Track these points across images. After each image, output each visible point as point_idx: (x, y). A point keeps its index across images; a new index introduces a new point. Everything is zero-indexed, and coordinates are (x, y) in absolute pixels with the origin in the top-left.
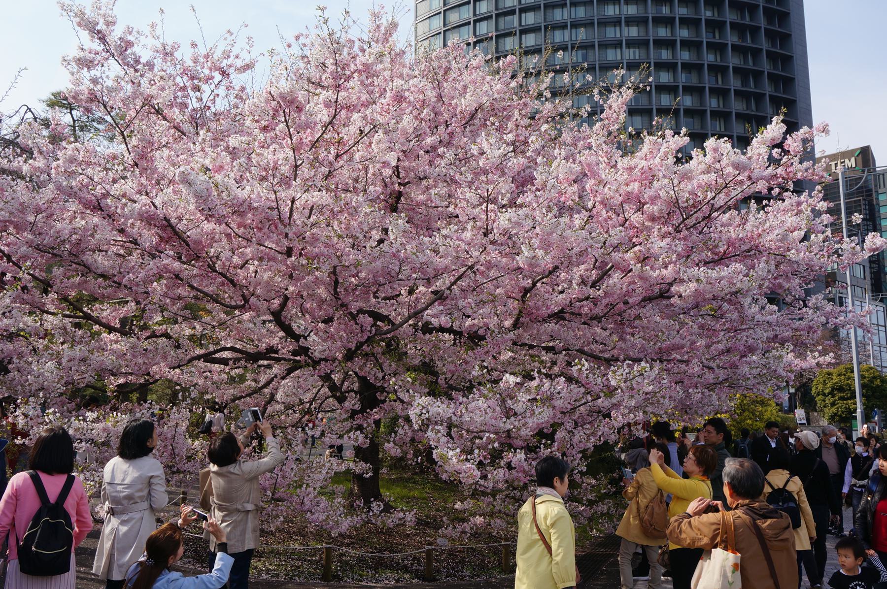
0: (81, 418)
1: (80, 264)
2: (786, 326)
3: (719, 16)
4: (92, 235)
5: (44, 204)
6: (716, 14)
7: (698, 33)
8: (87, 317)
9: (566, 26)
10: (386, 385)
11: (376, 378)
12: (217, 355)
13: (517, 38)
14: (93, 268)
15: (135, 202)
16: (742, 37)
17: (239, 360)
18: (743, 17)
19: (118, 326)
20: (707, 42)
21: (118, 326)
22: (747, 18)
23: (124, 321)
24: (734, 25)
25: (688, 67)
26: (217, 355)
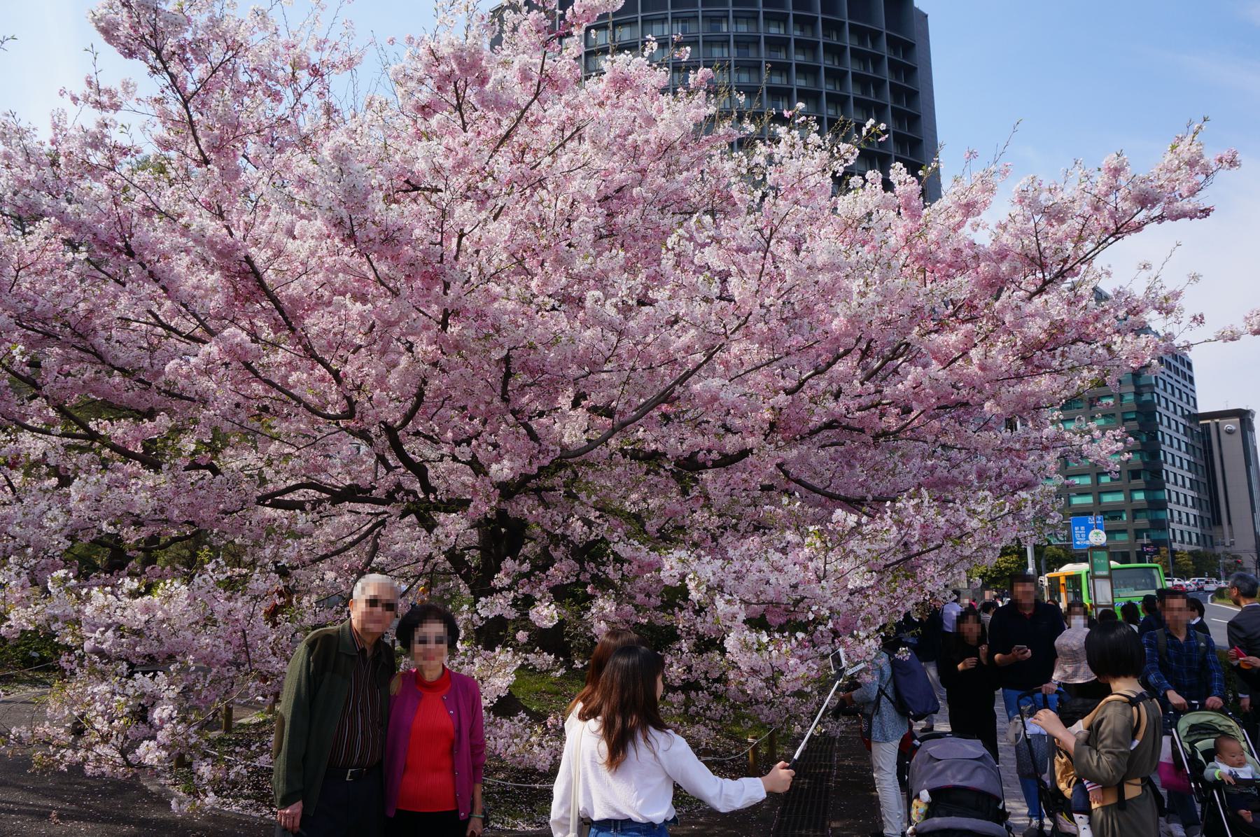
0: (108, 589)
1: (87, 351)
2: (50, 509)
3: (839, 65)
4: (113, 305)
5: (32, 252)
6: (838, 88)
7: (814, 33)
8: (93, 436)
9: (667, 18)
10: (568, 533)
11: (553, 524)
12: (287, 498)
13: (609, 33)
14: (109, 358)
15: (373, 326)
16: (865, 91)
17: (320, 502)
18: (866, 68)
19: (140, 450)
20: (824, 43)
21: (140, 450)
22: (871, 69)
23: (149, 445)
24: (858, 102)
25: (803, 70)
26: (287, 498)
